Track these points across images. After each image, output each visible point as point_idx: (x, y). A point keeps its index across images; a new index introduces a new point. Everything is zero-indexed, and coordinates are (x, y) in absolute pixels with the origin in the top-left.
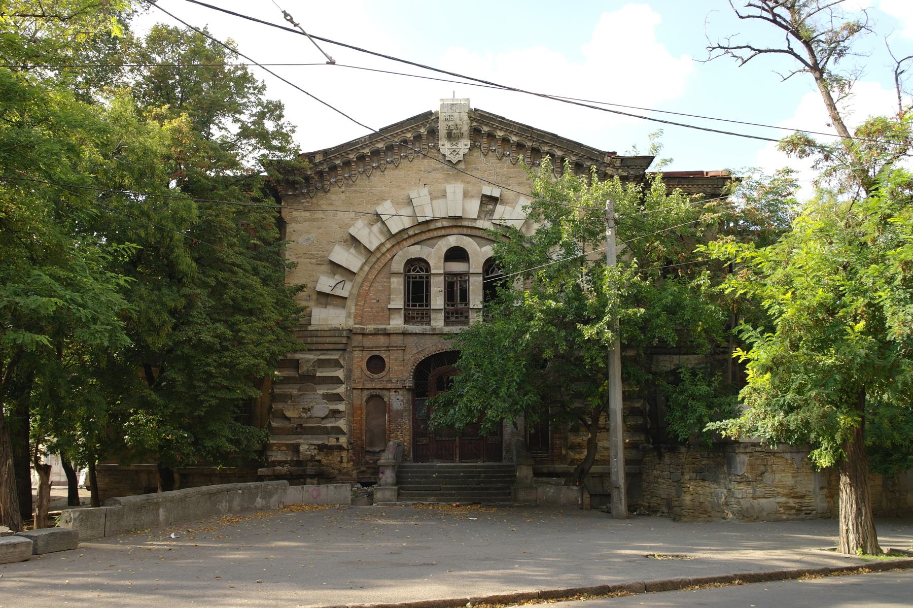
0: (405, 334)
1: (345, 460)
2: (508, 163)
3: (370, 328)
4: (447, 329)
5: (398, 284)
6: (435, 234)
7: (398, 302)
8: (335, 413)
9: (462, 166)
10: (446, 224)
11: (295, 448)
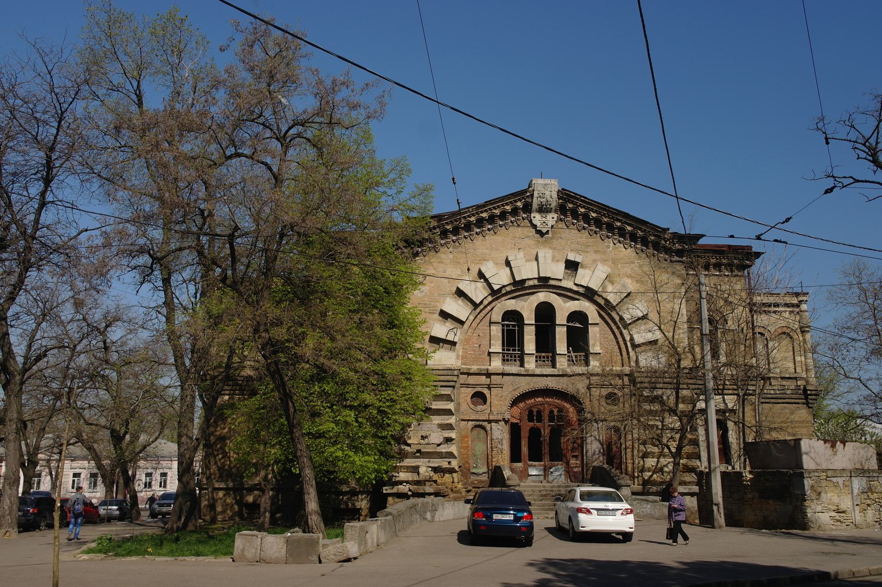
1: (456, 480)
3: (474, 368)
4: (538, 371)
5: (497, 331)
7: (497, 347)
8: (448, 440)
11: (415, 469)
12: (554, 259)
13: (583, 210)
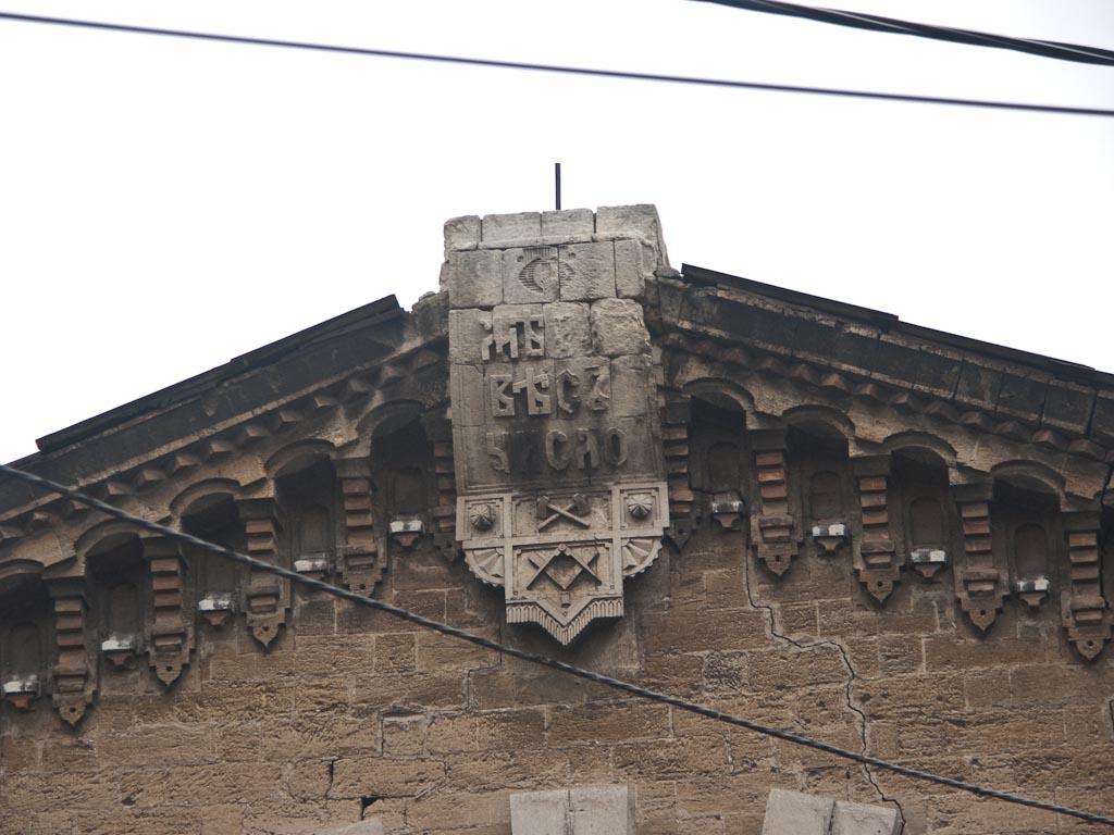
9: (623, 660)
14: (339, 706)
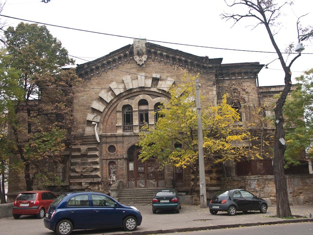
0: (123, 136)
1: (100, 188)
2: (163, 64)
5: (119, 116)
6: (133, 95)
7: (120, 123)
9: (144, 66)
10: (138, 90)
11: (80, 184)
12: (146, 77)
13: (159, 52)
14: (127, 69)
